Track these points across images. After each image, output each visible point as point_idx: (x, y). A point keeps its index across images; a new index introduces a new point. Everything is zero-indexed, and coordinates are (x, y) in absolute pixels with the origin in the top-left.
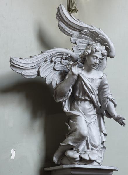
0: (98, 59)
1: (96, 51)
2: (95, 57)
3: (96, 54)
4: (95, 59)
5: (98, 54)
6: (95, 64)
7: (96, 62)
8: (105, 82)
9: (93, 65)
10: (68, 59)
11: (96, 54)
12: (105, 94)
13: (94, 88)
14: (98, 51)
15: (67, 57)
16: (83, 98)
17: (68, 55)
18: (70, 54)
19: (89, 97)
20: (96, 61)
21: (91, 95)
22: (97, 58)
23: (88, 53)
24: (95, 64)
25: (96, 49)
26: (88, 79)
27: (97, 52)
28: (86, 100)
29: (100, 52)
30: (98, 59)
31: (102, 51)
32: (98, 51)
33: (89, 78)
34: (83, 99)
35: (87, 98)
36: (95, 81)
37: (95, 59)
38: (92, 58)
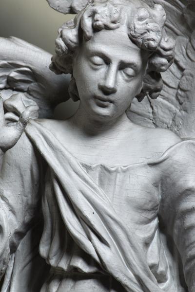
0: (114, 67)
1: (96, 29)
2: (98, 60)
3: (100, 44)
4: (103, 69)
5: (112, 43)
6: (100, 94)
7: (102, 83)
8: (181, 182)
9: (95, 97)
10: (23, 86)
11: (100, 44)
12: (30, 263)
13: (111, 212)
14: (107, 28)
15: (13, 74)
16: (64, 265)
17: (14, 66)
18: (23, 61)
19: (87, 258)
20: (106, 78)
21: (90, 246)
22: (107, 61)
23: (67, 44)
24: (100, 94)
25: (97, 16)
26: (83, 171)
27: (103, 34)
28: (76, 275)
29: (123, 32)
30: (114, 67)
31: (129, 28)
32: (107, 28)
33: (88, 168)
34: (63, 270)
35: (80, 264)
36: (119, 177)
37: (103, 69)
38: (85, 66)
